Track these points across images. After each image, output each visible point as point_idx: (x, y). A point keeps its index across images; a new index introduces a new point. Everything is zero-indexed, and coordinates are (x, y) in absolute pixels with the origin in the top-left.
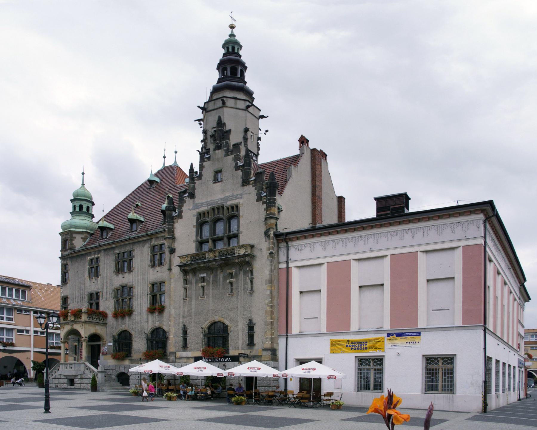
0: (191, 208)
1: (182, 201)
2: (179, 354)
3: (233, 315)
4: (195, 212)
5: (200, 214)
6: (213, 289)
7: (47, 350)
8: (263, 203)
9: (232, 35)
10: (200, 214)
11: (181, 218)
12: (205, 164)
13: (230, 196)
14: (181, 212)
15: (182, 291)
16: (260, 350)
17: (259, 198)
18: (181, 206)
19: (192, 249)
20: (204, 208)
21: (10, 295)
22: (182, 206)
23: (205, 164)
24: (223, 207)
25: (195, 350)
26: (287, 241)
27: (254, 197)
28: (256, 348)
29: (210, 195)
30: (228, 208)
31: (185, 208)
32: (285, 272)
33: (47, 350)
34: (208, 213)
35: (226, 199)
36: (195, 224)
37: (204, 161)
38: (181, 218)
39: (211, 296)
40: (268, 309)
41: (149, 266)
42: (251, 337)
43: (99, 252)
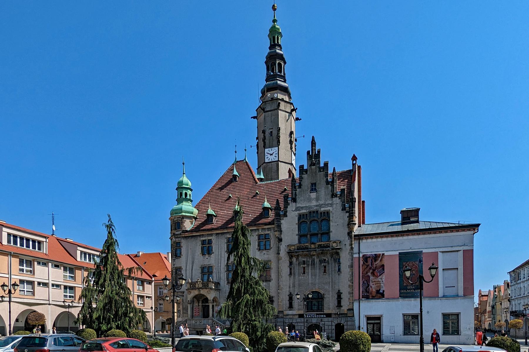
0: (294, 209)
1: (286, 204)
2: (286, 312)
3: (326, 287)
4: (297, 213)
5: (300, 215)
6: (311, 269)
7: (526, 341)
8: (347, 212)
9: (274, 27)
10: (300, 215)
11: (286, 216)
12: (303, 176)
13: (322, 204)
14: (286, 212)
15: (288, 270)
16: (346, 310)
17: (344, 209)
18: (286, 207)
19: (295, 240)
20: (303, 211)
21: (28, 246)
22: (287, 207)
23: (303, 176)
24: (317, 212)
25: (299, 310)
26: (359, 239)
27: (340, 208)
28: (342, 308)
29: (310, 201)
30: (321, 213)
31: (289, 209)
32: (357, 260)
33: (526, 341)
34: (306, 215)
35: (320, 206)
36: (297, 222)
37: (303, 174)
38: (286, 216)
39: (310, 274)
40: (351, 284)
41: (257, 249)
42: (339, 302)
43: (211, 235)
